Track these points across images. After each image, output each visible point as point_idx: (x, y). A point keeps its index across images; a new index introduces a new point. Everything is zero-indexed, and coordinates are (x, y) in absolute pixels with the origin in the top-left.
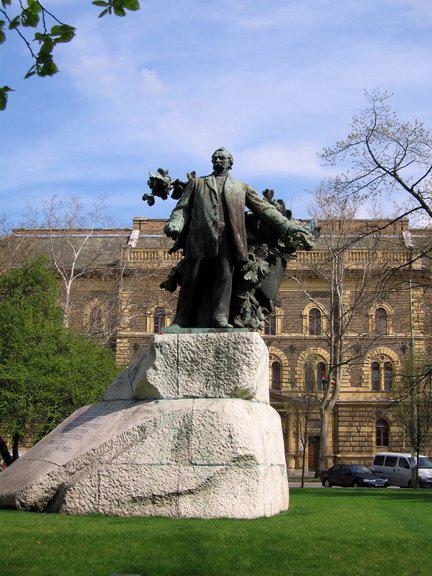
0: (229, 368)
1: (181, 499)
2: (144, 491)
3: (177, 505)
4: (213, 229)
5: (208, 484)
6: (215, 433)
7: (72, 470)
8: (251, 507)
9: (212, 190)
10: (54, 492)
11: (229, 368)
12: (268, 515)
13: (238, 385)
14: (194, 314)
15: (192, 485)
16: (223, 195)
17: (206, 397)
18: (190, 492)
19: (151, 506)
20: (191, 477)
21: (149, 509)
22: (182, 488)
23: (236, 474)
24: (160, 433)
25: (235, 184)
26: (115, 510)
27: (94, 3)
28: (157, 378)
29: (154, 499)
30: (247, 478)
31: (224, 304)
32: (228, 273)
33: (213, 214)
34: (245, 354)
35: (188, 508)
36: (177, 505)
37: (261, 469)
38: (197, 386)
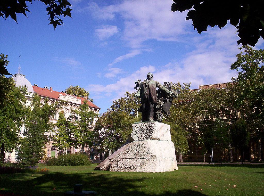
0: (150, 132)
1: (137, 167)
2: (128, 166)
3: (136, 169)
4: (146, 95)
5: (143, 164)
6: (145, 150)
7: (112, 160)
8: (155, 170)
9: (146, 84)
10: (109, 166)
11: (150, 132)
12: (162, 172)
13: (152, 137)
14: (145, 118)
15: (139, 164)
16: (148, 86)
17: (145, 140)
18: (139, 165)
19: (130, 169)
20: (139, 161)
21: (129, 170)
22: (137, 165)
23: (151, 161)
24: (132, 150)
25: (153, 82)
26: (122, 171)
27: (16, 20)
28: (133, 136)
29: (130, 167)
30: (154, 162)
31: (152, 114)
32: (152, 106)
33: (146, 91)
34: (153, 128)
35: (139, 170)
36: (136, 169)
37: (158, 159)
38: (143, 137)
